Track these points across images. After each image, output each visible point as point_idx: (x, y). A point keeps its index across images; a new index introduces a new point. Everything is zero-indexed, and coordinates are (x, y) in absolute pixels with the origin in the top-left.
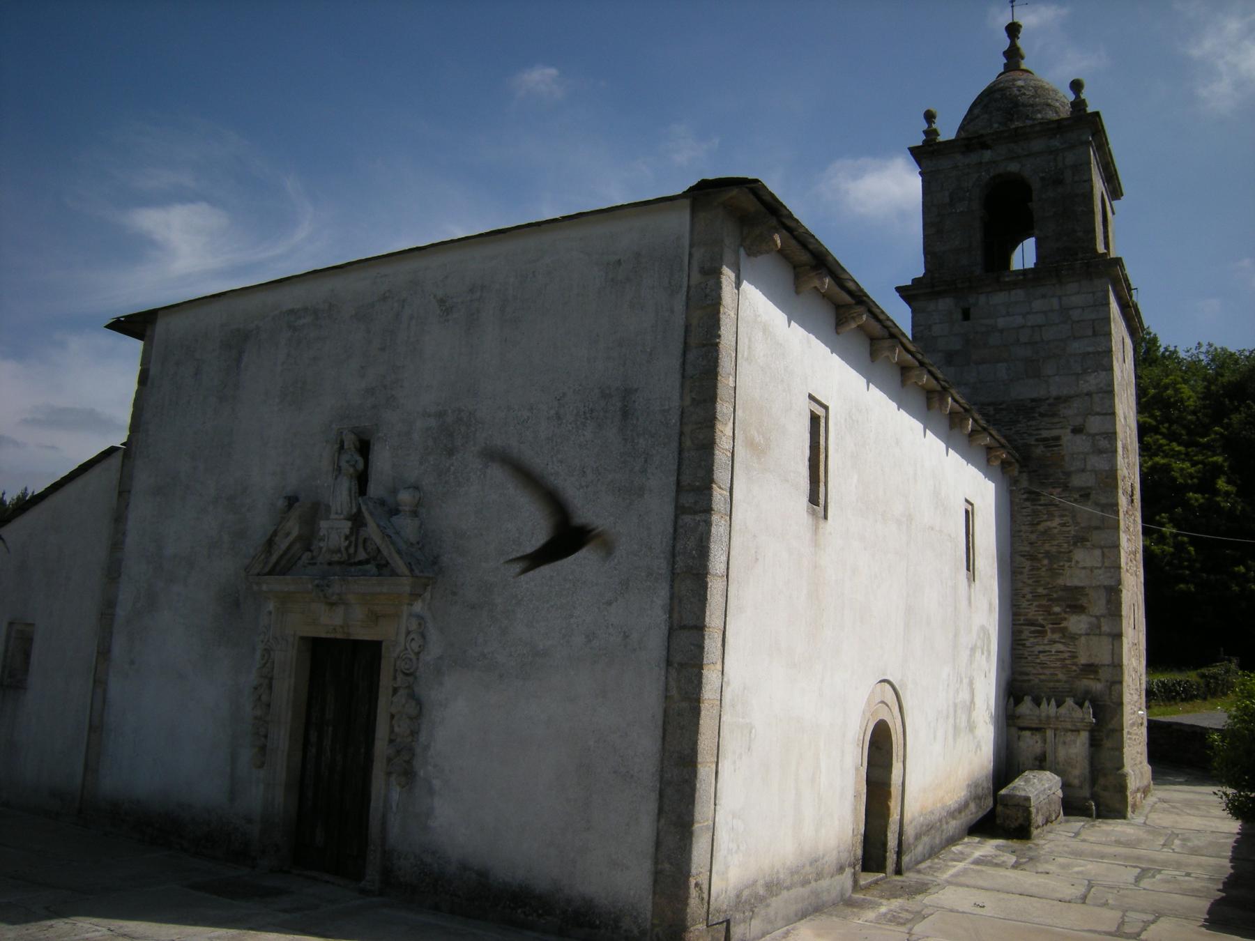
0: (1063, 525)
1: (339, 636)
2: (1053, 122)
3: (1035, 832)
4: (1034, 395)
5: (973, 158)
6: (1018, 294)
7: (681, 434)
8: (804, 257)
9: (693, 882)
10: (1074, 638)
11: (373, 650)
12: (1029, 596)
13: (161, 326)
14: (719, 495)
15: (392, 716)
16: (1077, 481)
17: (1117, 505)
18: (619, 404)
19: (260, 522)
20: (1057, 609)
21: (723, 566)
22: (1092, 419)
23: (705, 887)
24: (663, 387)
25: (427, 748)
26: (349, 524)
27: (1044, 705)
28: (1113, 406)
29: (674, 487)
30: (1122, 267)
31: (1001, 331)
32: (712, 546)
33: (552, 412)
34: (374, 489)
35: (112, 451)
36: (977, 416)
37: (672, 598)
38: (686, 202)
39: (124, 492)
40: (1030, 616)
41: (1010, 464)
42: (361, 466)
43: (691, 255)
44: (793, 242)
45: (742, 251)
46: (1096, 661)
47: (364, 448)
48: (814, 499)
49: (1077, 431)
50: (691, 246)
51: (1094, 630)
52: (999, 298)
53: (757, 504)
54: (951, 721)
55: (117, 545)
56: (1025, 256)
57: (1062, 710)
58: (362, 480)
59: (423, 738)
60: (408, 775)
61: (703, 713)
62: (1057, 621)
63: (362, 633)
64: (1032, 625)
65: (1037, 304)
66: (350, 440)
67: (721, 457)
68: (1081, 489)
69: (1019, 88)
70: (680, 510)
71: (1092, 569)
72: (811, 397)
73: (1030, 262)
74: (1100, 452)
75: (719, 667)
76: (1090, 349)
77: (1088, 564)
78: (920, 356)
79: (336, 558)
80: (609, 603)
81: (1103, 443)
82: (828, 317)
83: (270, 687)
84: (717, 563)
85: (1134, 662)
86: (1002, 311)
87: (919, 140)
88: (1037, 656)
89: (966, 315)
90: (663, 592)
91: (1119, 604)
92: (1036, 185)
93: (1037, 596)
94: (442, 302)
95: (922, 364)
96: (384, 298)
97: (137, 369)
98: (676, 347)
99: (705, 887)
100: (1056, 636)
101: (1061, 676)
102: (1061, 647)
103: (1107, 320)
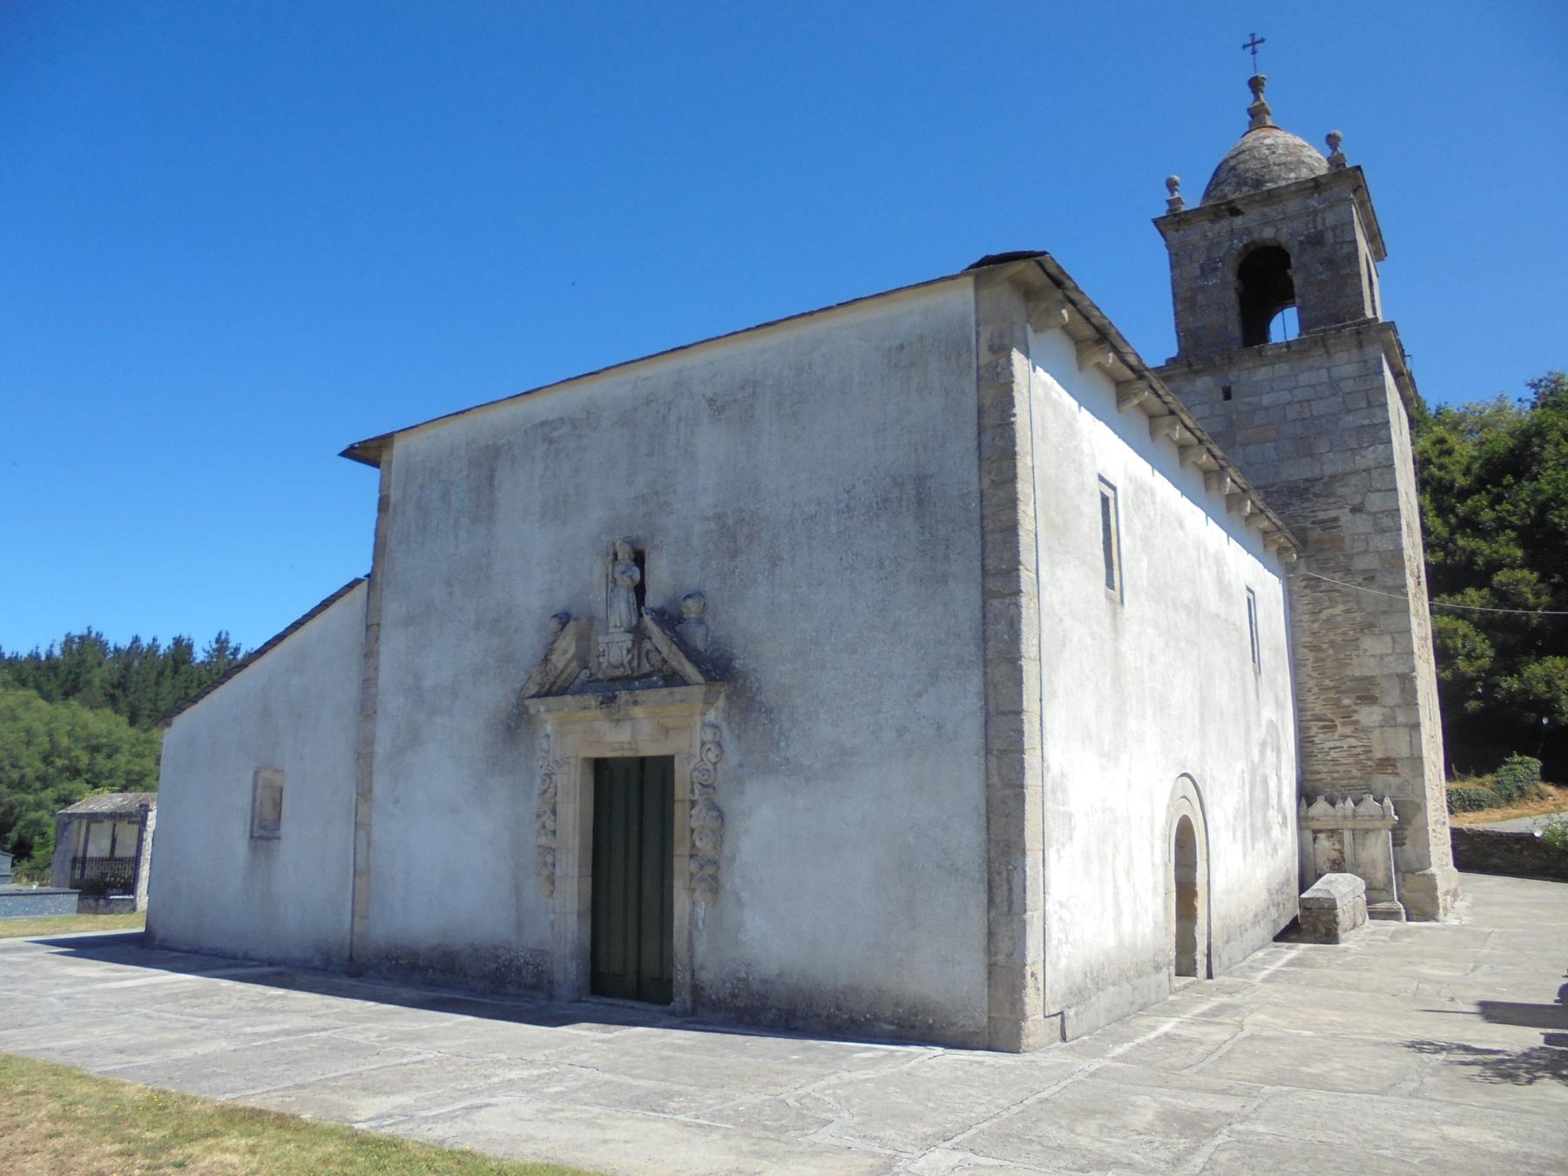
0: (1348, 611)
1: (628, 754)
2: (1307, 181)
3: (1342, 935)
4: (1309, 475)
5: (1224, 224)
6: (1282, 368)
7: (982, 517)
8: (1088, 332)
9: (1028, 970)
10: (1366, 730)
11: (665, 765)
12: (1315, 690)
13: (399, 446)
14: (1026, 576)
15: (693, 831)
16: (1360, 564)
17: (1405, 586)
18: (913, 492)
19: (529, 643)
20: (1346, 702)
21: (1035, 649)
22: (1372, 496)
23: (1040, 977)
24: (959, 466)
25: (733, 859)
26: (630, 637)
27: (1340, 805)
28: (1394, 481)
29: (979, 572)
30: (1396, 332)
31: (1266, 409)
32: (1024, 628)
33: (842, 505)
34: (653, 600)
35: (357, 582)
36: (1254, 497)
37: (986, 684)
38: (969, 281)
39: (372, 626)
40: (1317, 711)
41: (1286, 549)
42: (637, 577)
43: (978, 333)
44: (1078, 316)
45: (1029, 329)
46: (1394, 755)
47: (639, 559)
48: (1110, 583)
49: (1357, 510)
50: (978, 324)
51: (1389, 722)
52: (1262, 373)
53: (1058, 588)
54: (1248, 820)
55: (368, 682)
56: (1285, 326)
57: (1362, 809)
58: (640, 590)
59: (727, 850)
60: (714, 887)
61: (1028, 799)
62: (1347, 716)
63: (650, 749)
64: (1321, 720)
65: (1304, 378)
66: (624, 553)
67: (1025, 538)
68: (1365, 571)
69: (1269, 147)
70: (986, 594)
71: (1381, 657)
72: (1101, 479)
73: (1293, 332)
74: (1382, 531)
75: (1039, 752)
76: (1366, 422)
77: (1378, 652)
78: (1198, 433)
79: (618, 673)
80: (919, 695)
81: (1386, 522)
82: (1107, 392)
83: (554, 812)
84: (1028, 646)
85: (1433, 756)
86: (1263, 383)
87: (1162, 210)
88: (1328, 753)
89: (1227, 395)
90: (975, 683)
91: (1414, 692)
92: (1294, 252)
93: (1325, 689)
94: (711, 402)
95: (1200, 442)
96: (648, 403)
97: (376, 496)
98: (971, 431)
99: (1040, 977)
100: (1348, 730)
101: (1355, 773)
102: (1353, 742)
103: (1382, 389)
